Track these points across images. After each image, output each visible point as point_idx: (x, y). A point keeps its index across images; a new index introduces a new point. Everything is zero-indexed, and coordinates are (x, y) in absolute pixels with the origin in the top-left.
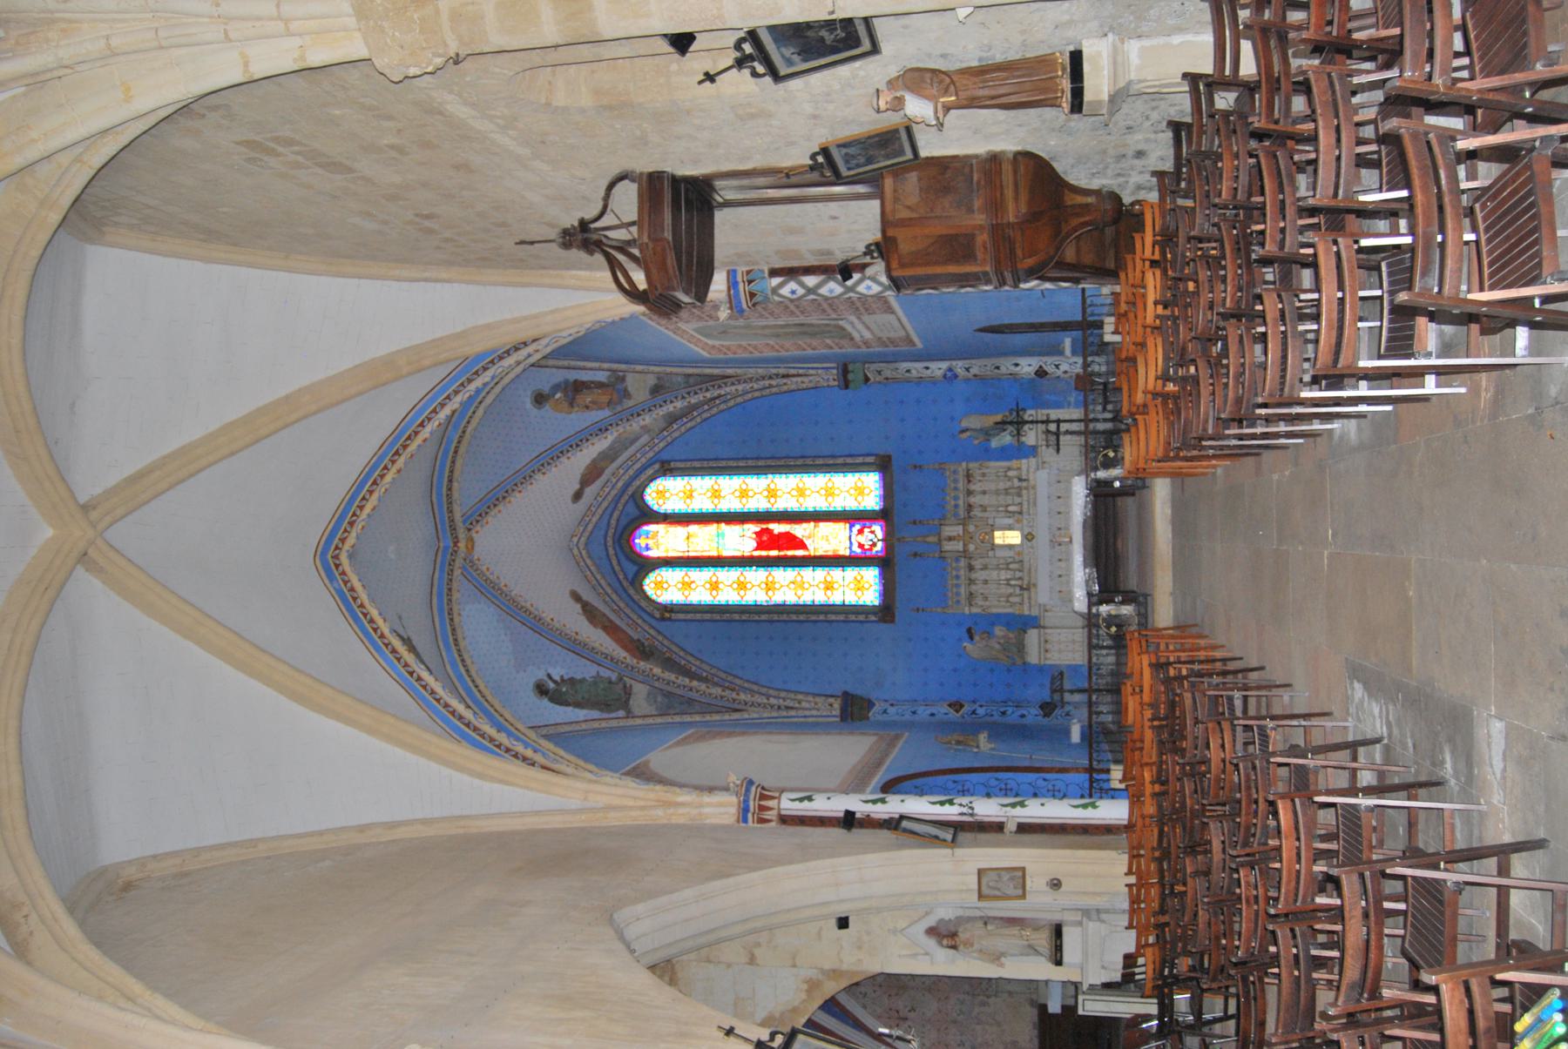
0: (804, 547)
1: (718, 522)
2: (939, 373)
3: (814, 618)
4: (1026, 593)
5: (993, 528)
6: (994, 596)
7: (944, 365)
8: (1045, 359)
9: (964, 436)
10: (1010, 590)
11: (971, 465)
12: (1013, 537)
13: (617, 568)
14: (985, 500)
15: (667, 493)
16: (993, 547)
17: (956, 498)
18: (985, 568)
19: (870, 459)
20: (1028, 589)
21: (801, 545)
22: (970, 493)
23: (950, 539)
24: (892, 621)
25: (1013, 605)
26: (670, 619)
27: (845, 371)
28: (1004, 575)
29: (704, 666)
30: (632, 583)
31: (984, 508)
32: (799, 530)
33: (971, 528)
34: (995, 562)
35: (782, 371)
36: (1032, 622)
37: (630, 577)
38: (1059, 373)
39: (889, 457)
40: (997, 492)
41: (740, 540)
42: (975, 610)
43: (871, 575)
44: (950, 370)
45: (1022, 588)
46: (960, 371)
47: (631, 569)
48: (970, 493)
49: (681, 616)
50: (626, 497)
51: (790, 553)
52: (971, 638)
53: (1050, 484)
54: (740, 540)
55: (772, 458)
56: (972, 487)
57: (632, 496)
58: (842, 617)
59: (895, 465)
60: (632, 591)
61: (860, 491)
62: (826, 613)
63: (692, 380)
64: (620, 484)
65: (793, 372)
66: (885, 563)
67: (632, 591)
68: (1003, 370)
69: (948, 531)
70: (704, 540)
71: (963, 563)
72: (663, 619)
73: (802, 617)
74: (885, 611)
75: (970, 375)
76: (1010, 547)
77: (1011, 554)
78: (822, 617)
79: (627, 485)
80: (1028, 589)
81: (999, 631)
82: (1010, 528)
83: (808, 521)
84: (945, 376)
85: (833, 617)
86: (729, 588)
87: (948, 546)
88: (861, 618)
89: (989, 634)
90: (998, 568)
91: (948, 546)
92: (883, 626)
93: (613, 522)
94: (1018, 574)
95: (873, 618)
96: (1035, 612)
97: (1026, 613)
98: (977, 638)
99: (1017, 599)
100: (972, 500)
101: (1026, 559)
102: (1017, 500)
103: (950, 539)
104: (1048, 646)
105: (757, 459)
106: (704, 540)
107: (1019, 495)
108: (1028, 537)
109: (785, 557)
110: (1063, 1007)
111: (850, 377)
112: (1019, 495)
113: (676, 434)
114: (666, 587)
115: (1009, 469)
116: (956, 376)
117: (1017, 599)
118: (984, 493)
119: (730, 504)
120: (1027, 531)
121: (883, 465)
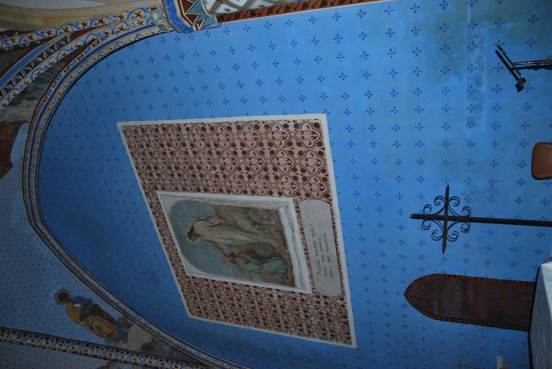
63: (175, 354)
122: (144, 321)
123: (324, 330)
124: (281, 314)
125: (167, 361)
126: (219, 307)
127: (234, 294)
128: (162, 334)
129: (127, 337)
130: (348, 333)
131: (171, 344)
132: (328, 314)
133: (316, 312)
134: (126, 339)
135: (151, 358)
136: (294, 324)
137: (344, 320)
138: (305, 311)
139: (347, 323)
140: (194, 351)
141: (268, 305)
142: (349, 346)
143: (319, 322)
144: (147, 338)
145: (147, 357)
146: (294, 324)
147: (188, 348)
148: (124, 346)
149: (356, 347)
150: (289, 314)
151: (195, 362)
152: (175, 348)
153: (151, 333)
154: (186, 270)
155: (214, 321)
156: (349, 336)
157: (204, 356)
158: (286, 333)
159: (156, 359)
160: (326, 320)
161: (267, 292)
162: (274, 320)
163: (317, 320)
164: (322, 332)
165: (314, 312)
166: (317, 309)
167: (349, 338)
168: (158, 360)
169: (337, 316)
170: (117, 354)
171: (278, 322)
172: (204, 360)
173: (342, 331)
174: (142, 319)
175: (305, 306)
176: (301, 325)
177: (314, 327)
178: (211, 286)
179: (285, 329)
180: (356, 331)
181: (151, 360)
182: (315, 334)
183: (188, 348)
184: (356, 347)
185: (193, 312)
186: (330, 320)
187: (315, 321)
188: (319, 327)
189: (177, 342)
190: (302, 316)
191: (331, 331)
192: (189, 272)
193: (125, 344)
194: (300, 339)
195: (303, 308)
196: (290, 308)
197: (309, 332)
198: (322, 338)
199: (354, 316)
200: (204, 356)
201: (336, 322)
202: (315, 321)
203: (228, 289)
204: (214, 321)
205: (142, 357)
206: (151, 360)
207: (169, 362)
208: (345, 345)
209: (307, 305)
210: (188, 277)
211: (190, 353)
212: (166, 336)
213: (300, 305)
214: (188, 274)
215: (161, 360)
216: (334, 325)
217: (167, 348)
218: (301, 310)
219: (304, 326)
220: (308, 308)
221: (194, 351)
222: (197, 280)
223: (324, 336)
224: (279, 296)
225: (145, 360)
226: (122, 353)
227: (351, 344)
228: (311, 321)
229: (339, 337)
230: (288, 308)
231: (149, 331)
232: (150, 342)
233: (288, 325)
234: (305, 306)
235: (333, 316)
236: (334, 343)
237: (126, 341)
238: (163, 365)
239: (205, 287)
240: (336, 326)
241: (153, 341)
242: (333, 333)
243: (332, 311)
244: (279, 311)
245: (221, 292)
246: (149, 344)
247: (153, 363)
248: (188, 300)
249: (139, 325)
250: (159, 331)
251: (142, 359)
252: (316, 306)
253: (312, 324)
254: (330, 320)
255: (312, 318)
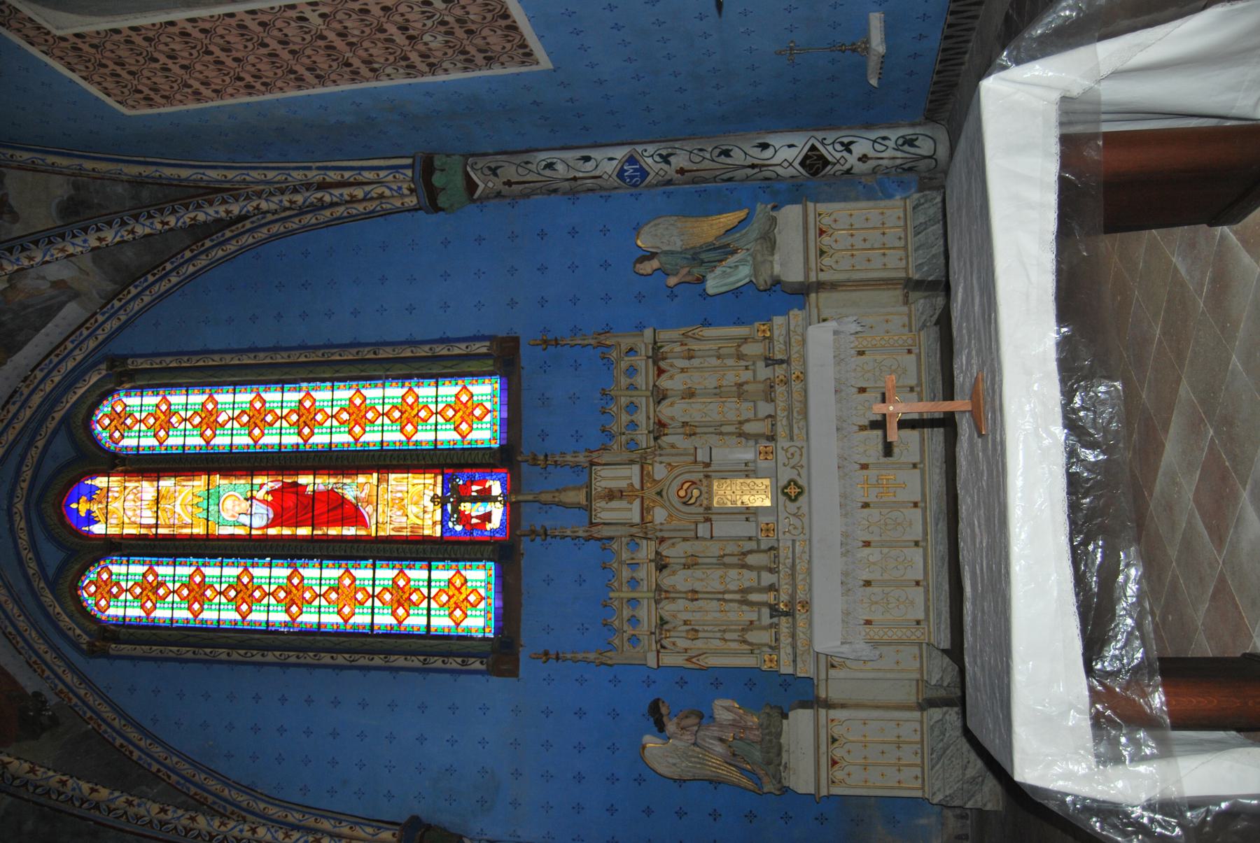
0: (359, 520)
1: (209, 472)
2: (610, 168)
3: (363, 661)
4: (784, 622)
5: (709, 472)
6: (709, 628)
7: (620, 153)
8: (820, 135)
9: (647, 267)
10: (750, 615)
11: (664, 335)
12: (759, 496)
13: (27, 555)
14: (694, 411)
15: (138, 417)
16: (709, 514)
17: (632, 408)
18: (691, 563)
19: (481, 348)
20: (790, 614)
21: (352, 514)
22: (660, 396)
23: (611, 495)
24: (514, 673)
25: (753, 648)
26: (105, 655)
27: (427, 168)
28: (736, 579)
29: (157, 750)
30: (53, 586)
31: (690, 430)
32: (354, 488)
33: (659, 472)
34: (714, 549)
35: (314, 176)
36: (804, 694)
37: (51, 572)
38: (852, 160)
39: (516, 341)
40: (719, 392)
41: (240, 507)
42: (668, 660)
43: (479, 576)
44: (631, 160)
45: (774, 611)
46: (649, 162)
47: (53, 556)
48: (660, 396)
49: (126, 649)
50: (51, 425)
51: (333, 531)
52: (661, 727)
53: (839, 360)
54: (240, 507)
55: (303, 347)
56: (664, 383)
57: (64, 420)
58: (416, 662)
59: (527, 355)
60: (48, 598)
61: (465, 412)
62: (388, 652)
63: (145, 194)
64: (37, 399)
65: (334, 176)
66: (502, 552)
67: (48, 598)
68: (738, 157)
69: (607, 478)
70: (182, 505)
71: (647, 550)
72: (93, 652)
73: (341, 659)
74: (500, 652)
75: (671, 171)
76: (750, 513)
77: (749, 529)
78: (378, 661)
79: (52, 401)
80: (790, 614)
81: (724, 709)
82: (748, 471)
83: (367, 470)
84: (621, 174)
85: (400, 661)
86: (219, 599)
87: (607, 512)
88: (454, 663)
89: (703, 717)
90: (721, 562)
91: (607, 512)
92: (495, 680)
93: (27, 474)
94: (767, 579)
95: (477, 665)
96: (805, 669)
97: (786, 669)
98: (671, 727)
99: (764, 637)
100: (666, 411)
101: (785, 544)
102: (765, 409)
103: (611, 495)
104: (838, 753)
105: (276, 349)
106: (182, 505)
107: (769, 397)
108: (791, 492)
109: (327, 539)
110: (770, 320)
111: (438, 180)
112: (769, 397)
113: (136, 306)
114: (122, 595)
115: (745, 340)
116: (644, 174)
117: (764, 637)
118: (690, 394)
119: (613, 528)
120: (785, 475)
121: (503, 360)
122: (26, 156)
123: (464, 52)
124: (348, 48)
125: (136, 218)
126: (186, 77)
127: (207, 41)
128: (88, 165)
129: (10, 206)
130: (524, 45)
131: (125, 178)
132: (460, 21)
133: (429, 23)
134: (12, 211)
135: (99, 230)
136: (387, 60)
137: (504, 23)
138: (403, 29)
139: (513, 28)
140: (184, 173)
141: (304, 39)
142: (534, 68)
143: (447, 42)
144: (60, 189)
145: (85, 230)
146: (387, 60)
147: (168, 172)
148: (17, 230)
149: (550, 66)
150: (366, 44)
151: (201, 191)
152: (138, 183)
153: (61, 173)
154: (45, 25)
155: (193, 106)
156: (527, 50)
157: (213, 174)
158: (377, 79)
159: (110, 224)
160: (460, 33)
161: (286, 14)
162: (335, 64)
163: (440, 38)
164: (462, 57)
165: (424, 25)
166: (429, 18)
167: (530, 54)
168: (116, 226)
169: (484, 18)
170: (13, 258)
171: (348, 65)
172: (217, 181)
173: (508, 46)
174: (18, 153)
175: (398, 18)
176: (406, 58)
177: (439, 54)
178: (138, 40)
179: (371, 74)
180: (541, 37)
181: (102, 235)
182: (446, 65)
183: (168, 172)
184: (550, 66)
185: (130, 102)
186: (470, 32)
187: (435, 42)
188: (450, 52)
189: (134, 170)
190: (400, 39)
191: (480, 51)
192: (57, 28)
193: (18, 225)
194: (416, 84)
195: (395, 23)
196: (363, 32)
197: (431, 65)
198: (466, 69)
199: (526, 8)
200: (213, 174)
201: (486, 32)
202: (435, 42)
203: (184, 34)
204: (193, 106)
205: (74, 236)
206: (102, 235)
207: (142, 220)
208: (524, 69)
209: (402, 15)
210: (63, 39)
211: (179, 179)
212: (103, 166)
213: (383, 20)
214: (59, 33)
215: (123, 223)
216: (484, 38)
217: (119, 189)
218: (392, 29)
219: (414, 57)
220: (407, 21)
221: (184, 173)
222: (91, 37)
223: (469, 63)
224: (322, 16)
225: (85, 241)
226: (24, 249)
227: (538, 63)
228: (426, 44)
229: (504, 58)
230: (357, 32)
231: (54, 170)
232: (73, 192)
233: (376, 66)
234: (398, 18)
235: (473, 22)
236: (497, 71)
237: (15, 217)
238: (132, 232)
239: (122, 46)
240: (489, 40)
241: (76, 187)
242: (489, 54)
243: (468, 13)
244: (339, 43)
245: (172, 46)
246: (71, 198)
247: (109, 239)
248: (99, 84)
249: (19, 168)
250: (77, 161)
251: (78, 241)
252: (423, 12)
253: (430, 49)
254: (470, 32)
255: (427, 38)
